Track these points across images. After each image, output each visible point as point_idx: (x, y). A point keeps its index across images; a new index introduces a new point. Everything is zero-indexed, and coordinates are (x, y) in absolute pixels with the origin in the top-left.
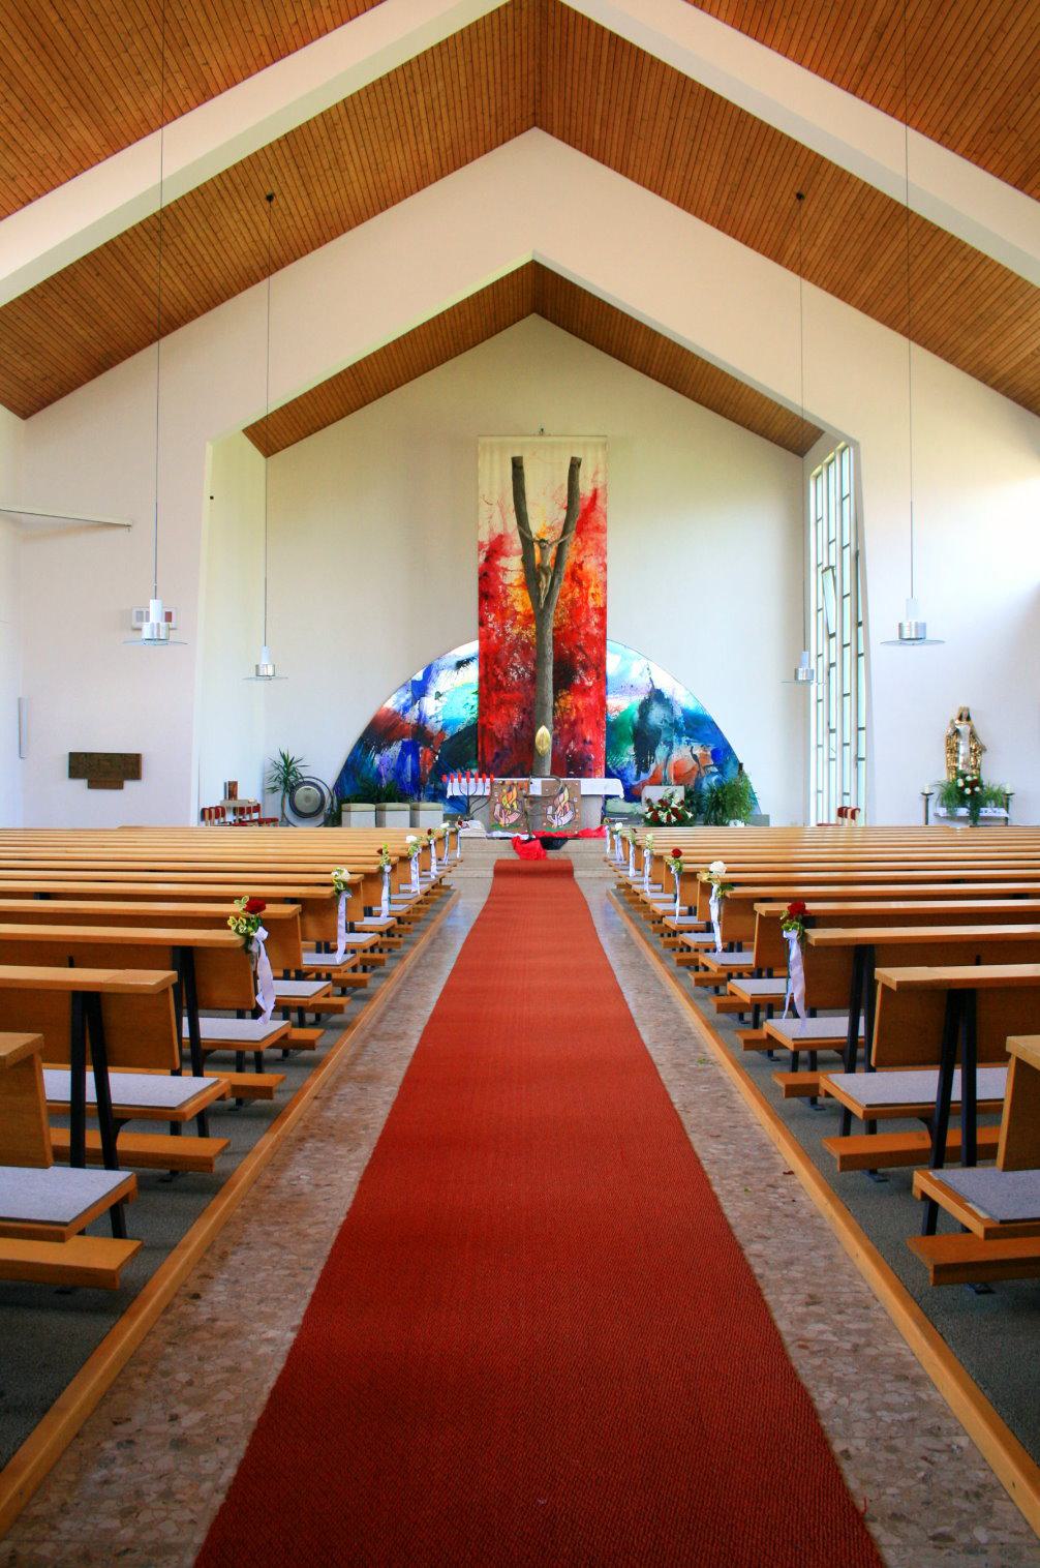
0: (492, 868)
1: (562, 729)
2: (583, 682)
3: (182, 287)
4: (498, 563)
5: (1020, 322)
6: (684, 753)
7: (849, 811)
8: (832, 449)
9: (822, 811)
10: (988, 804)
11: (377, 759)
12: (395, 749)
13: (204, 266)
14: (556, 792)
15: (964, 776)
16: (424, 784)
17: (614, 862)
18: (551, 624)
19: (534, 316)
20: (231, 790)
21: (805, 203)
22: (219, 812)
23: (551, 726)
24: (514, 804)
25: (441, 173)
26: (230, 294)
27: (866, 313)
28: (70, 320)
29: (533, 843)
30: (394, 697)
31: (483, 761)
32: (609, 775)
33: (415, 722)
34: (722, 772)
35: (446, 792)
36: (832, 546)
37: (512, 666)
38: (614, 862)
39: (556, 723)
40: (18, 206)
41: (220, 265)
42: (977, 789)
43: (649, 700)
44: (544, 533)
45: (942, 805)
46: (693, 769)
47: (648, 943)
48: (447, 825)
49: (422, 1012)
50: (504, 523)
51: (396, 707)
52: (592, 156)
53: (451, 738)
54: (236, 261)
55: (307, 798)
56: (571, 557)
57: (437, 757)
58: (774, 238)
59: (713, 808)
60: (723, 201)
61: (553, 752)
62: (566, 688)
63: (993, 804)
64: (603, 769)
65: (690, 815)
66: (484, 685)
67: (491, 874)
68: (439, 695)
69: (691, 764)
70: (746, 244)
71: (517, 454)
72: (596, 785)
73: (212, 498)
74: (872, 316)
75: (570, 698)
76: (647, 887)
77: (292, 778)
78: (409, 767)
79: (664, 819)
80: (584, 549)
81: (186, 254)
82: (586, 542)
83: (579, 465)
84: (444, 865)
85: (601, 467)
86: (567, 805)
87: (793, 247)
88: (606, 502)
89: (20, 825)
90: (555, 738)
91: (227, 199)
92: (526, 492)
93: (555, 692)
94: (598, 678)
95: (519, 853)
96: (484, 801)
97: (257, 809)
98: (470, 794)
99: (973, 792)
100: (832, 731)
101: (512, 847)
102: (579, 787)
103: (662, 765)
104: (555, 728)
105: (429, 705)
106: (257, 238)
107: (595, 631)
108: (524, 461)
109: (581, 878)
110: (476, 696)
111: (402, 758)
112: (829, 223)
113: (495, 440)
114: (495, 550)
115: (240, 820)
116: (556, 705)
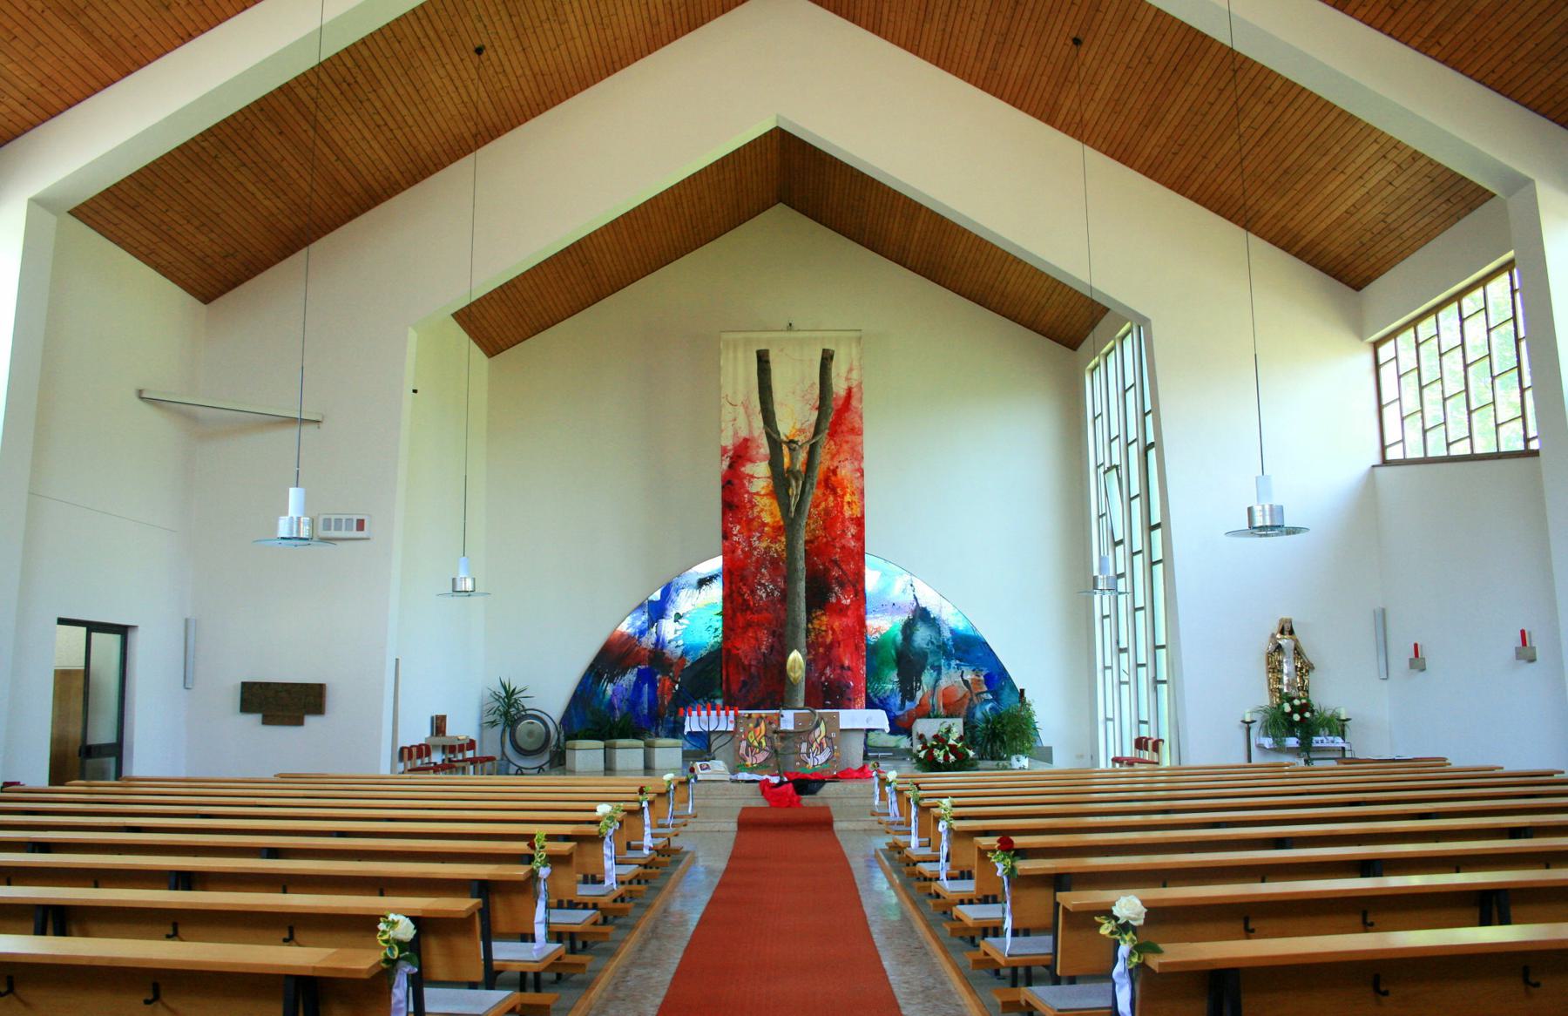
0: (736, 820)
2: (839, 600)
3: (382, 154)
4: (743, 469)
5: (1335, 173)
6: (953, 678)
7: (1150, 743)
8: (1112, 337)
9: (1114, 743)
10: (1321, 732)
11: (610, 689)
12: (630, 677)
13: (407, 130)
14: (810, 725)
15: (1290, 700)
19: (780, 207)
20: (439, 725)
21: (1083, 50)
22: (423, 750)
23: (804, 650)
24: (763, 741)
25: (674, 35)
26: (439, 166)
27: (1151, 177)
28: (252, 188)
29: (784, 786)
30: (629, 620)
31: (728, 689)
32: (870, 705)
33: (652, 646)
34: (997, 698)
35: (684, 727)
36: (1115, 444)
37: (760, 584)
40: (176, 42)
41: (426, 130)
42: (1307, 715)
43: (913, 619)
45: (1266, 735)
46: (965, 696)
47: (945, 951)
49: (676, 956)
50: (750, 424)
51: (631, 631)
52: (841, 15)
53: (692, 664)
54: (444, 126)
55: (530, 734)
56: (823, 461)
57: (677, 687)
58: (1047, 95)
59: (989, 740)
60: (989, 54)
63: (1327, 733)
65: (971, 753)
66: (729, 605)
67: (734, 826)
68: (678, 617)
69: (962, 690)
70: (1014, 105)
71: (763, 347)
72: (854, 718)
73: (415, 391)
74: (1158, 181)
75: (824, 618)
77: (513, 711)
78: (645, 699)
80: (838, 452)
81: (385, 115)
82: (841, 446)
85: (855, 363)
86: (824, 741)
87: (1068, 103)
89: (183, 774)
90: (808, 664)
91: (429, 49)
92: (774, 390)
93: (809, 612)
94: (856, 596)
96: (727, 738)
97: (471, 745)
98: (711, 729)
99: (1303, 719)
100: (1121, 651)
101: (760, 793)
103: (930, 692)
104: (809, 653)
105: (668, 628)
106: (466, 99)
107: (853, 543)
109: (842, 831)
111: (637, 687)
112: (1110, 72)
114: (740, 455)
115: (450, 760)
116: (810, 626)
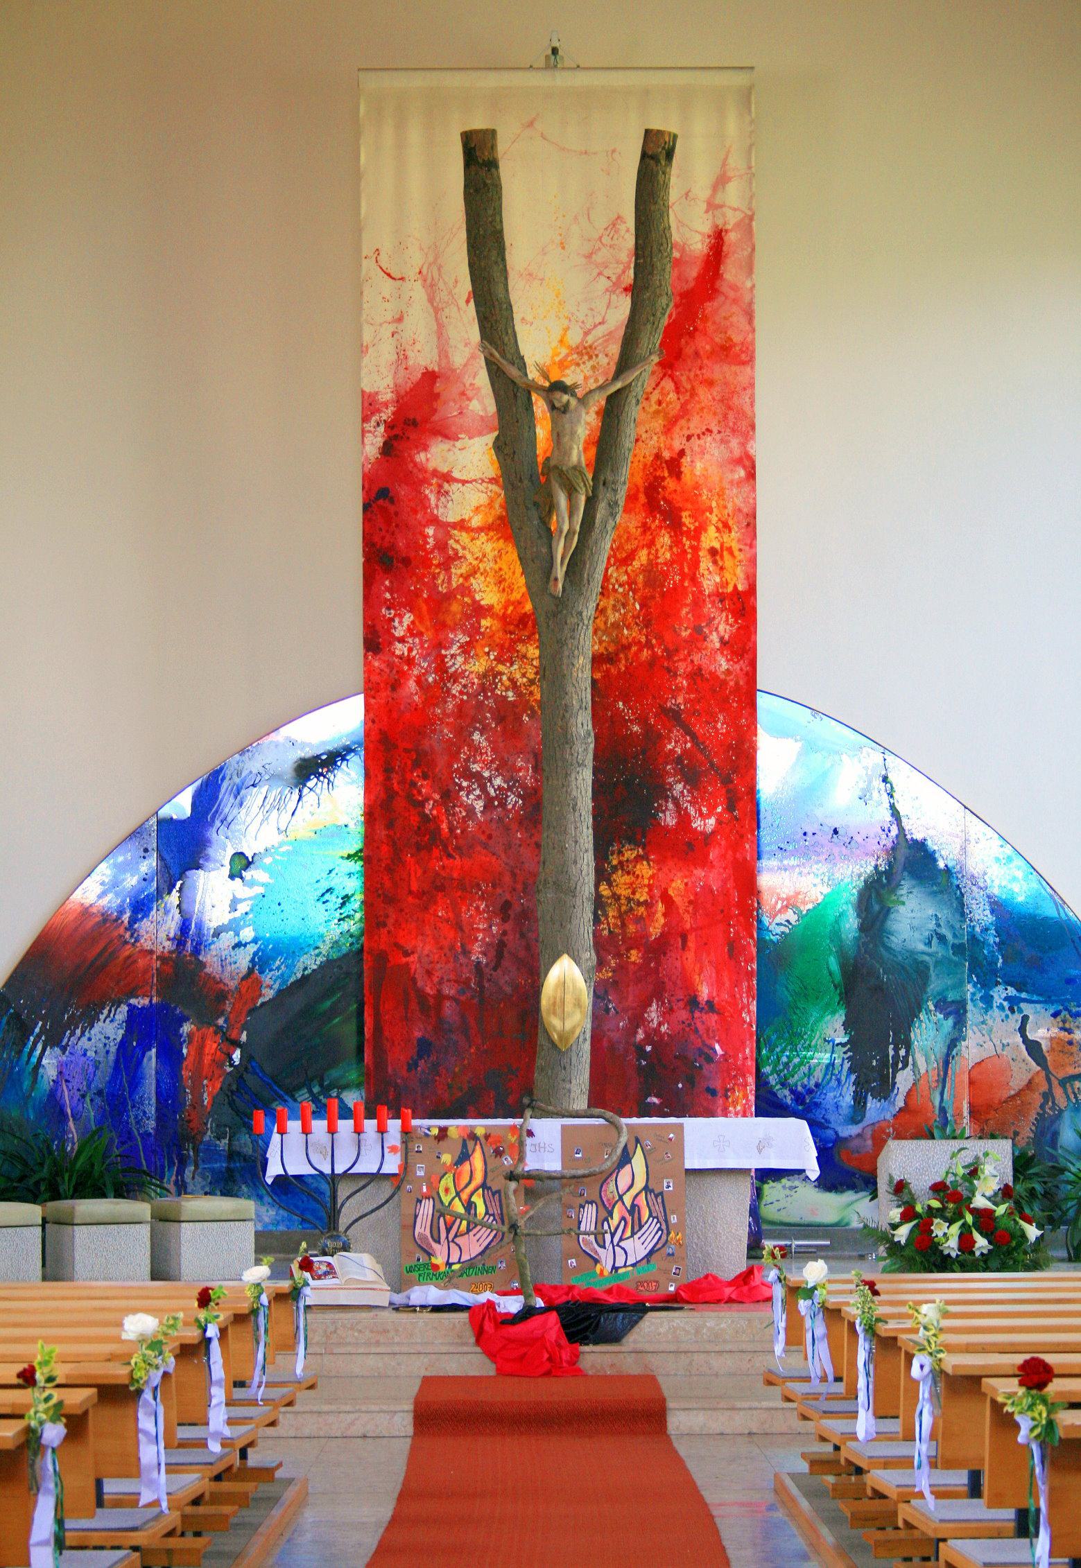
1: (622, 968)
2: (684, 819)
4: (421, 457)
16: (194, 1139)
17: (798, 1388)
18: (586, 644)
23: (590, 956)
29: (534, 1323)
30: (104, 871)
31: (380, 1064)
32: (768, 1106)
35: (265, 1163)
37: (468, 775)
38: (798, 1388)
39: (602, 945)
43: (889, 873)
44: (562, 365)
46: (1030, 1085)
48: (262, 1271)
51: (110, 902)
57: (237, 1056)
61: (597, 1039)
62: (634, 841)
64: (751, 1087)
65: (1032, 1232)
66: (382, 833)
67: (404, 1424)
68: (242, 864)
69: (1023, 1069)
71: (478, 123)
75: (645, 870)
76: (923, 1480)
78: (149, 1086)
79: (951, 1245)
80: (684, 412)
82: (693, 394)
83: (670, 154)
84: (253, 1402)
85: (736, 162)
88: (750, 270)
90: (600, 993)
94: (730, 808)
95: (491, 1354)
96: (387, 1188)
98: (339, 1169)
102: (677, 1146)
103: (933, 1076)
104: (601, 964)
108: (502, 147)
110: (357, 866)
111: (127, 1058)
113: (418, 81)
116: (605, 890)
